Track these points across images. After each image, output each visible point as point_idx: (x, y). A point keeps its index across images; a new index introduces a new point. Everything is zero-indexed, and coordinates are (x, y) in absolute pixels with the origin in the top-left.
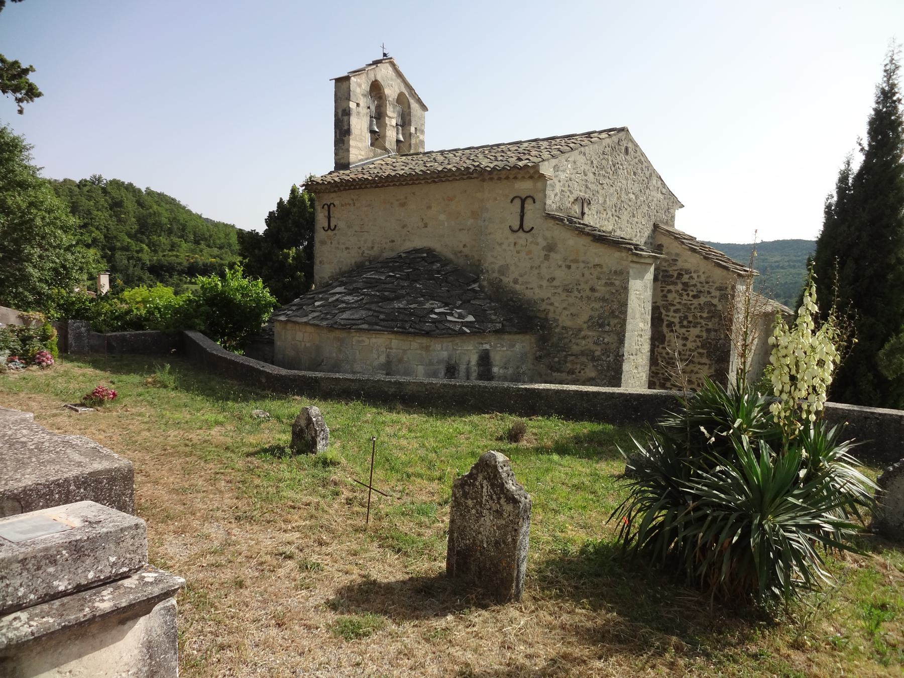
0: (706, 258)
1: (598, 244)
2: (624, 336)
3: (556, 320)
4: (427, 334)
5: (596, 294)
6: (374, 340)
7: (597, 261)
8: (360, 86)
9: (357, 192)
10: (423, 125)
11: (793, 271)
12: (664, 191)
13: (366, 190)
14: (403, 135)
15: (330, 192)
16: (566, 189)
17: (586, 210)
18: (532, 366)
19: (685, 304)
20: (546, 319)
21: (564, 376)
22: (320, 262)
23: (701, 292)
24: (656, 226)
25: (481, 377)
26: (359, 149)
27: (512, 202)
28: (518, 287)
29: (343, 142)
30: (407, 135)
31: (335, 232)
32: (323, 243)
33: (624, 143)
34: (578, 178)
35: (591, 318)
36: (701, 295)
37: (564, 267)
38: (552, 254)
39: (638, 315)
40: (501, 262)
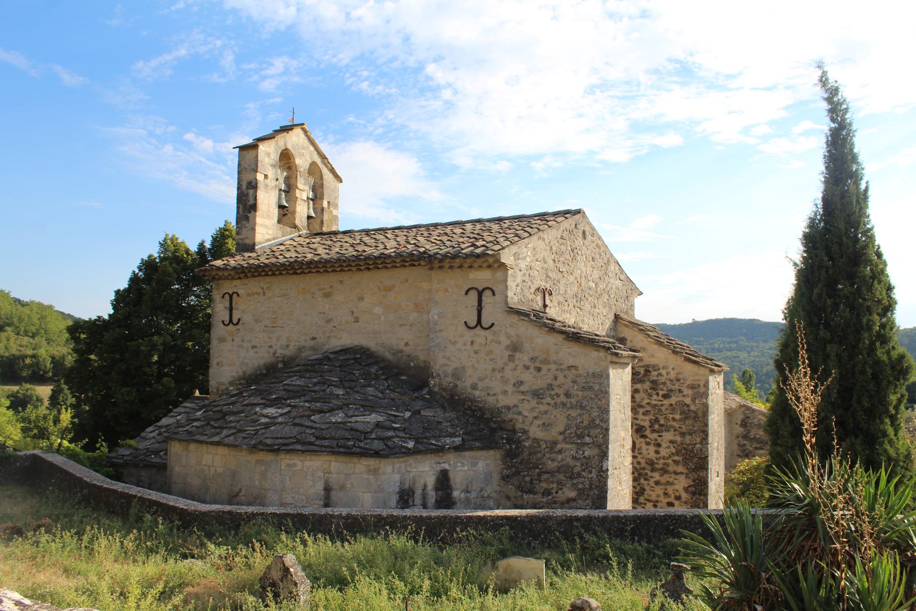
0: (674, 352)
1: (572, 343)
2: (607, 448)
3: (525, 432)
4: (377, 454)
5: (573, 401)
6: (308, 463)
7: (571, 362)
8: (268, 155)
9: (268, 279)
10: (336, 198)
11: (729, 354)
12: (622, 277)
13: (280, 277)
14: (314, 209)
15: (233, 279)
16: (527, 278)
17: (548, 302)
18: (498, 488)
19: (656, 405)
20: (514, 431)
21: (539, 498)
22: (218, 364)
23: (672, 390)
24: (617, 317)
25: (439, 505)
26: (266, 227)
27: (466, 294)
28: (477, 393)
29: (247, 219)
30: (319, 210)
31: (237, 327)
32: (222, 340)
33: (581, 227)
34: (538, 265)
35: (568, 427)
36: (672, 394)
37: (532, 370)
38: (518, 355)
39: (619, 423)
40: (457, 365)
